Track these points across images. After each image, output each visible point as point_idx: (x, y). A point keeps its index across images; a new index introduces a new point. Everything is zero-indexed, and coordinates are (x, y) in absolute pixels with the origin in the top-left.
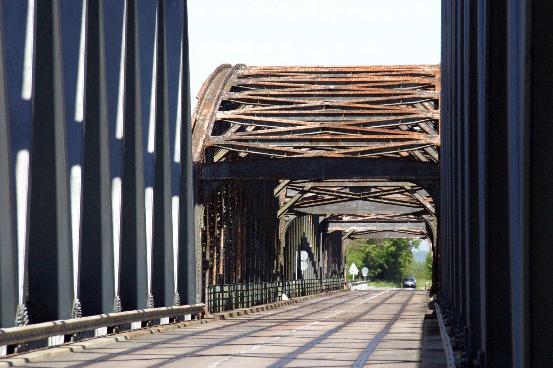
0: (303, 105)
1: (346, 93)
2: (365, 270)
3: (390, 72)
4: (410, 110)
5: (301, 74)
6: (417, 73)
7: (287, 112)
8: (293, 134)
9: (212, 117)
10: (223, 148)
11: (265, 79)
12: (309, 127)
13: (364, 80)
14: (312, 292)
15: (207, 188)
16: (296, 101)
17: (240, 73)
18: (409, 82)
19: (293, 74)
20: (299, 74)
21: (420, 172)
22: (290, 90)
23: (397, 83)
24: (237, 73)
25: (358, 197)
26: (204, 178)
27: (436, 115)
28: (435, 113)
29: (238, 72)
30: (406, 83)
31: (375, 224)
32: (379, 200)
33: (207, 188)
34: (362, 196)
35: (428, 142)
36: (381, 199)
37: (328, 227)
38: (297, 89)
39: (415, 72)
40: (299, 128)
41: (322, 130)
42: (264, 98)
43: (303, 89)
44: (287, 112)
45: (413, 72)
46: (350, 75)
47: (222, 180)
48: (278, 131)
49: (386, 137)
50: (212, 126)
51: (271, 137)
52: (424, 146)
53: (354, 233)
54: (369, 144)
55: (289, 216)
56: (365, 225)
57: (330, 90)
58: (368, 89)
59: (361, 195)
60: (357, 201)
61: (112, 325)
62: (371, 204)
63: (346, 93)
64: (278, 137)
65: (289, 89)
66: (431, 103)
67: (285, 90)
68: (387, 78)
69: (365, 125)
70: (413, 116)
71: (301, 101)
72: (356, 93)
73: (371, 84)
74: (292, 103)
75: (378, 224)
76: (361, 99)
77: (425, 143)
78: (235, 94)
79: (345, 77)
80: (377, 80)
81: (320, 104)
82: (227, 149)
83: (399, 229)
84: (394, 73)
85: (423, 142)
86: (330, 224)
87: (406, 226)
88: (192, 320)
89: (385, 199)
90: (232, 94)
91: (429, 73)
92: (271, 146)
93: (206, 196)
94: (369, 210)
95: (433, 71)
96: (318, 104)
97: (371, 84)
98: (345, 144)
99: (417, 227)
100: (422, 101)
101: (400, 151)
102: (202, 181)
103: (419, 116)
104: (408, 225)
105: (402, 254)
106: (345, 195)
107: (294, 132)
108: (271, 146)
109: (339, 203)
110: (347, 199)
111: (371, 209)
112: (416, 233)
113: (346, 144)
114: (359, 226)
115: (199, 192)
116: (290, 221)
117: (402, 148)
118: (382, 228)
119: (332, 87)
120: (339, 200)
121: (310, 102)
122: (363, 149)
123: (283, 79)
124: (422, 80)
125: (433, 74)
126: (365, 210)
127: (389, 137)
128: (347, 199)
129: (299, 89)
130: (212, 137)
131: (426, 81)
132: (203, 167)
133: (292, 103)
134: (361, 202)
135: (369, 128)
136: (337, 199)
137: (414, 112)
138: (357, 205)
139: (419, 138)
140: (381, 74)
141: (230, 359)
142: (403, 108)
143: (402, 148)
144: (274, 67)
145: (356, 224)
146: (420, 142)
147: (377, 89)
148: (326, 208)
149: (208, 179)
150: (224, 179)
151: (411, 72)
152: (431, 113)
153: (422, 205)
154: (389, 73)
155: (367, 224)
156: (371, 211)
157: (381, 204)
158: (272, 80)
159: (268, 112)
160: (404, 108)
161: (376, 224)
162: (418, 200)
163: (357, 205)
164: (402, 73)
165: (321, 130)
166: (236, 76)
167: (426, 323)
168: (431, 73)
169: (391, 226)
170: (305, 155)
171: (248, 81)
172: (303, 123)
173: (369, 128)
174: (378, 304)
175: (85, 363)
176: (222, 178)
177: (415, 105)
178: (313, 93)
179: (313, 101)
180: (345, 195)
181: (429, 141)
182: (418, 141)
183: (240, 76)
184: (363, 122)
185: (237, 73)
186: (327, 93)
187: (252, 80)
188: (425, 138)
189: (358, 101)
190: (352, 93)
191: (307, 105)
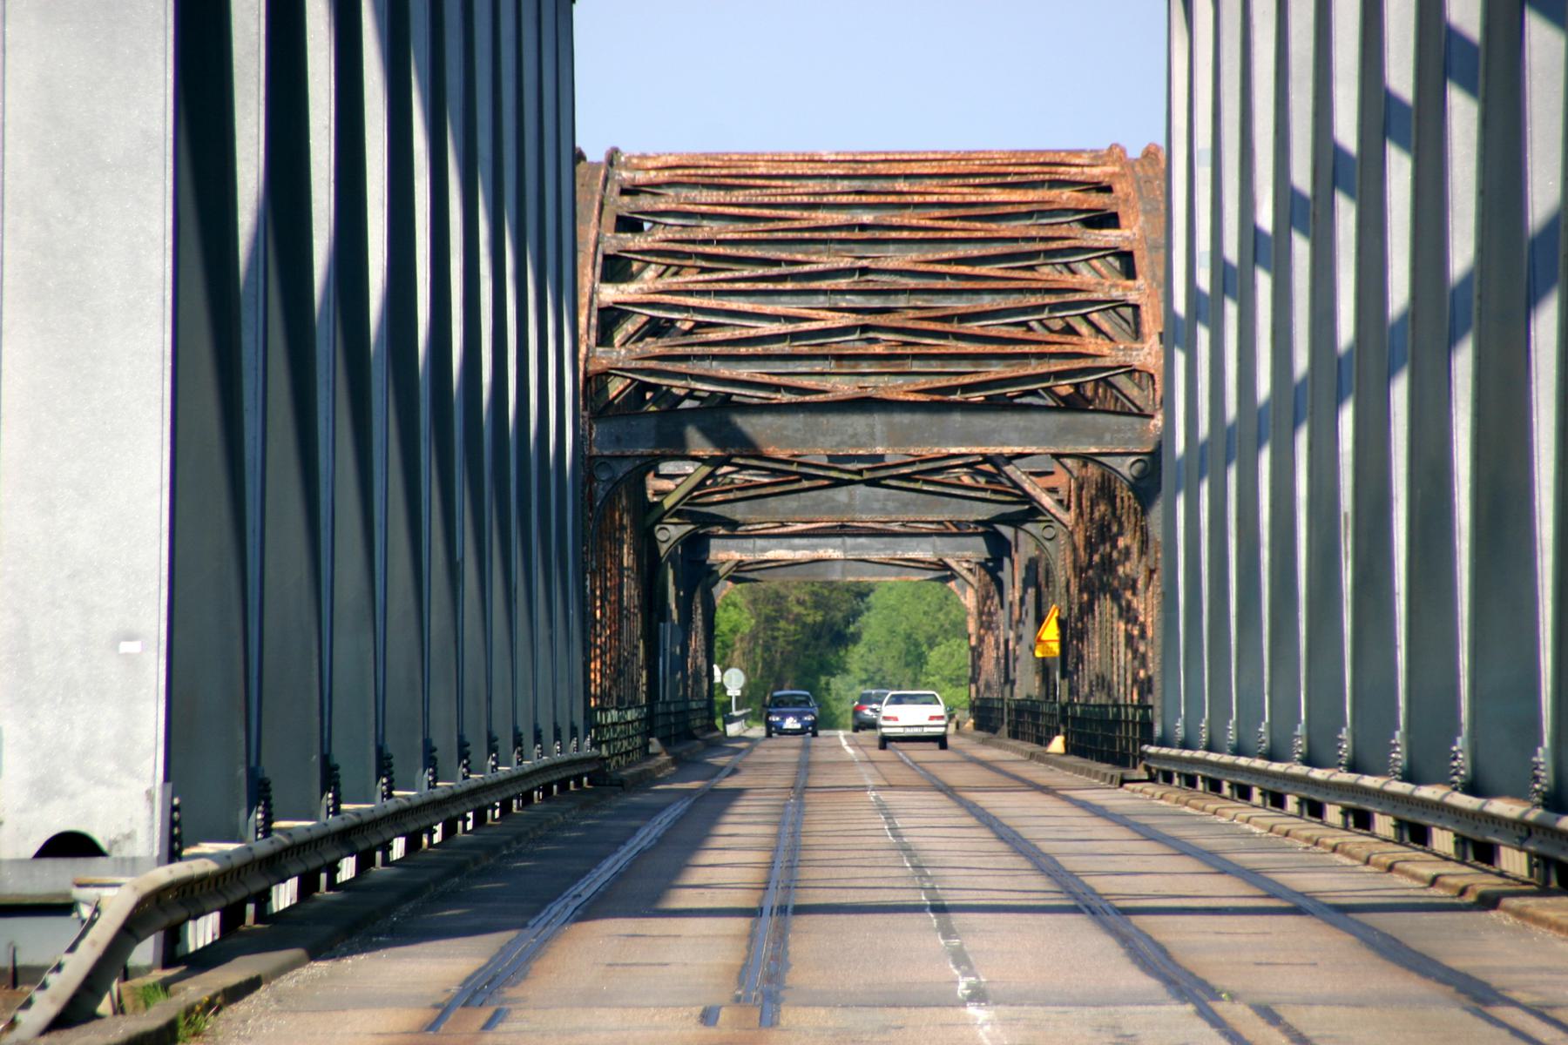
0: (807, 268)
1: (905, 234)
2: (733, 677)
4: (1069, 280)
5: (779, 183)
6: (1067, 178)
7: (771, 286)
8: (791, 342)
9: (591, 301)
10: (616, 375)
12: (829, 324)
13: (943, 198)
14: (673, 739)
15: (604, 476)
16: (784, 256)
17: (624, 180)
18: (1055, 206)
19: (759, 182)
20: (774, 183)
21: (1108, 437)
22: (766, 228)
23: (1024, 209)
24: (617, 177)
25: (857, 478)
26: (595, 451)
27: (1133, 293)
28: (1131, 290)
29: (620, 175)
30: (1047, 207)
31: (838, 541)
32: (912, 485)
33: (604, 476)
34: (867, 475)
35: (1122, 363)
36: (917, 481)
37: (707, 550)
38: (782, 225)
39: (1062, 177)
40: (805, 326)
41: (862, 332)
42: (708, 249)
43: (796, 224)
44: (771, 286)
45: (1057, 177)
47: (641, 456)
48: (758, 334)
49: (1018, 349)
50: (594, 321)
51: (743, 350)
52: (1112, 373)
53: (740, 565)
54: (980, 366)
55: (668, 527)
56: (812, 546)
57: (863, 227)
58: (956, 224)
59: (865, 472)
60: (851, 487)
62: (890, 494)
63: (905, 234)
65: (762, 224)
66: (1108, 262)
67: (755, 227)
68: (997, 195)
69: (965, 318)
70: (1078, 297)
71: (799, 257)
72: (930, 235)
73: (961, 212)
74: (777, 263)
75: (849, 541)
76: (946, 251)
77: (1114, 364)
78: (633, 240)
79: (892, 189)
80: (973, 199)
81: (848, 265)
82: (627, 377)
83: (907, 556)
84: (1009, 179)
85: (1108, 362)
86: (713, 542)
87: (928, 547)
89: (926, 482)
90: (627, 239)
91: (1096, 180)
92: (744, 372)
93: (601, 493)
94: (884, 510)
95: (1105, 175)
96: (842, 265)
97: (961, 212)
98: (920, 367)
99: (958, 550)
100: (1091, 255)
101: (1055, 383)
102: (592, 458)
103: (1095, 296)
104: (934, 547)
105: (868, 623)
106: (821, 473)
107: (795, 336)
108: (744, 372)
109: (802, 494)
110: (826, 482)
111: (888, 508)
112: (922, 565)
113: (923, 367)
114: (794, 548)
115: (584, 485)
116: (671, 542)
118: (861, 552)
119: (867, 217)
120: (806, 484)
121: (821, 260)
122: (967, 380)
124: (1085, 201)
125: (1106, 181)
126: (871, 511)
127: (1027, 349)
128: (826, 482)
129: (782, 225)
130: (600, 350)
131: (1096, 200)
132: (594, 426)
133: (777, 263)
134: (862, 490)
135: (973, 327)
136: (799, 481)
137: (1077, 286)
138: (851, 497)
139: (1099, 353)
140: (977, 181)
142: (1044, 274)
145: (786, 541)
146: (1099, 363)
147: (978, 225)
148: (769, 506)
149: (606, 453)
150: (645, 453)
151: (1053, 177)
152: (1120, 289)
153: (1027, 498)
154: (999, 180)
155: (815, 541)
156: (889, 513)
157: (914, 495)
158: (715, 199)
159: (725, 286)
160: (1048, 273)
161: (844, 544)
162: (1016, 485)
163: (851, 497)
164: (1031, 178)
165: (858, 332)
166: (617, 189)
167: (778, 864)
168: (1101, 179)
169: (886, 549)
170: (830, 395)
171: (655, 203)
172: (813, 313)
173: (973, 327)
176: (640, 451)
177: (1073, 266)
178: (824, 235)
179: (828, 257)
180: (821, 473)
181: (1123, 359)
182: (1099, 359)
183: (626, 186)
184: (959, 312)
185: (617, 177)
187: (663, 200)
188: (1114, 353)
189: (937, 256)
190: (920, 235)
191: (814, 267)
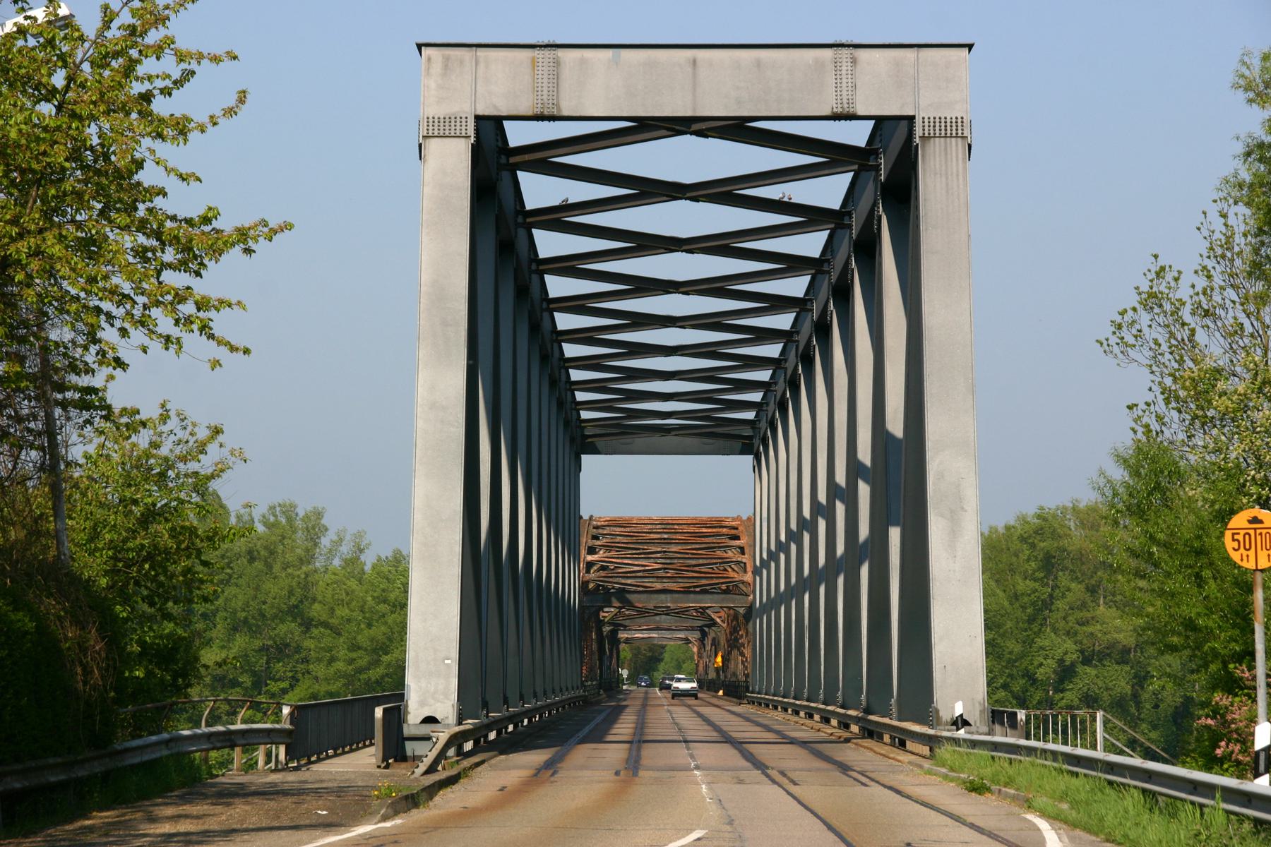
3: (703, 524)
11: (615, 529)
40: (647, 568)
46: (676, 527)
57: (665, 539)
61: (478, 736)
64: (633, 575)
74: (639, 549)
88: (726, 697)
92: (629, 581)
108: (629, 581)
117: (722, 583)
119: (666, 536)
123: (628, 529)
131: (733, 532)
133: (639, 549)
135: (697, 569)
141: (242, 821)
143: (722, 583)
144: (633, 518)
160: (719, 553)
173: (697, 569)
174: (285, 793)
175: (111, 830)
186: (662, 541)
